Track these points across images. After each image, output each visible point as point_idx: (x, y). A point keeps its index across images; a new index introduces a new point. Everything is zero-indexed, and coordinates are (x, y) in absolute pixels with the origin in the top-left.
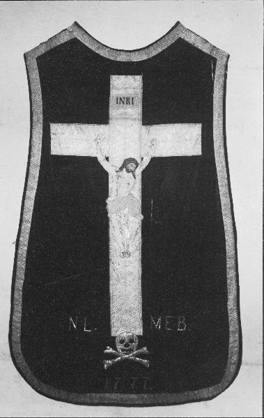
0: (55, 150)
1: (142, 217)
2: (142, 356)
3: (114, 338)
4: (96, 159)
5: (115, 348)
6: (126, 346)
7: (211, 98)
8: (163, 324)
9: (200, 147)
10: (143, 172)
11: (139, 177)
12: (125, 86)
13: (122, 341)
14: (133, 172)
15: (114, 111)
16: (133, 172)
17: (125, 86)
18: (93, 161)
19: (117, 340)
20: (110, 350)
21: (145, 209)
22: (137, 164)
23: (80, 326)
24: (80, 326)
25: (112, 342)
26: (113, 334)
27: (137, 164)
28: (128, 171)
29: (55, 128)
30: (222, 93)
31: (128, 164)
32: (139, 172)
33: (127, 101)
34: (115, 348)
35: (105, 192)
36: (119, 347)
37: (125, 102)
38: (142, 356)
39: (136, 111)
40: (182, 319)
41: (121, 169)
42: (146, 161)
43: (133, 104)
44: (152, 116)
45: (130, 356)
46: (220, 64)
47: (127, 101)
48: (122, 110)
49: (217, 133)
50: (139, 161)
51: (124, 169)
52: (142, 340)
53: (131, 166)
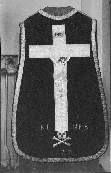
5: (57, 137)
7: (26, 34)
8: (78, 127)
10: (68, 63)
11: (66, 64)
12: (58, 29)
14: (64, 62)
16: (64, 62)
17: (58, 29)
19: (58, 134)
20: (55, 138)
21: (68, 77)
22: (65, 59)
23: (46, 127)
25: (55, 134)
26: (56, 130)
32: (66, 62)
33: (59, 35)
34: (57, 137)
36: (59, 136)
38: (43, 129)
39: (63, 39)
40: (86, 125)
41: (59, 61)
42: (69, 58)
43: (62, 36)
44: (69, 41)
46: (94, 22)
47: (59, 35)
48: (58, 39)
50: (66, 58)
51: (60, 61)
53: (63, 60)
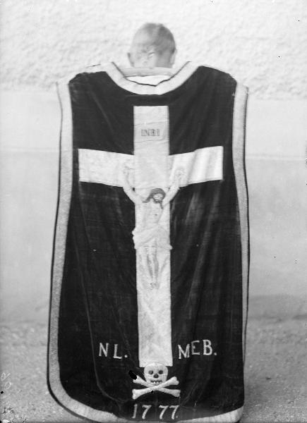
0: (84, 177)
1: (170, 247)
2: (182, 355)
3: (143, 369)
4: (121, 189)
6: (156, 376)
9: (87, 180)
13: (151, 373)
14: (160, 202)
15: (138, 140)
16: (160, 202)
18: (119, 191)
24: (111, 352)
27: (164, 195)
28: (156, 202)
29: (83, 153)
30: (242, 114)
31: (155, 195)
32: (166, 201)
35: (131, 224)
37: (151, 134)
38: (171, 387)
41: (148, 199)
45: (160, 387)
49: (237, 155)
50: (165, 190)
51: (152, 200)
52: (172, 372)
